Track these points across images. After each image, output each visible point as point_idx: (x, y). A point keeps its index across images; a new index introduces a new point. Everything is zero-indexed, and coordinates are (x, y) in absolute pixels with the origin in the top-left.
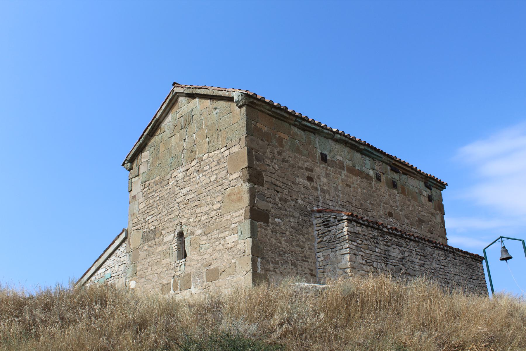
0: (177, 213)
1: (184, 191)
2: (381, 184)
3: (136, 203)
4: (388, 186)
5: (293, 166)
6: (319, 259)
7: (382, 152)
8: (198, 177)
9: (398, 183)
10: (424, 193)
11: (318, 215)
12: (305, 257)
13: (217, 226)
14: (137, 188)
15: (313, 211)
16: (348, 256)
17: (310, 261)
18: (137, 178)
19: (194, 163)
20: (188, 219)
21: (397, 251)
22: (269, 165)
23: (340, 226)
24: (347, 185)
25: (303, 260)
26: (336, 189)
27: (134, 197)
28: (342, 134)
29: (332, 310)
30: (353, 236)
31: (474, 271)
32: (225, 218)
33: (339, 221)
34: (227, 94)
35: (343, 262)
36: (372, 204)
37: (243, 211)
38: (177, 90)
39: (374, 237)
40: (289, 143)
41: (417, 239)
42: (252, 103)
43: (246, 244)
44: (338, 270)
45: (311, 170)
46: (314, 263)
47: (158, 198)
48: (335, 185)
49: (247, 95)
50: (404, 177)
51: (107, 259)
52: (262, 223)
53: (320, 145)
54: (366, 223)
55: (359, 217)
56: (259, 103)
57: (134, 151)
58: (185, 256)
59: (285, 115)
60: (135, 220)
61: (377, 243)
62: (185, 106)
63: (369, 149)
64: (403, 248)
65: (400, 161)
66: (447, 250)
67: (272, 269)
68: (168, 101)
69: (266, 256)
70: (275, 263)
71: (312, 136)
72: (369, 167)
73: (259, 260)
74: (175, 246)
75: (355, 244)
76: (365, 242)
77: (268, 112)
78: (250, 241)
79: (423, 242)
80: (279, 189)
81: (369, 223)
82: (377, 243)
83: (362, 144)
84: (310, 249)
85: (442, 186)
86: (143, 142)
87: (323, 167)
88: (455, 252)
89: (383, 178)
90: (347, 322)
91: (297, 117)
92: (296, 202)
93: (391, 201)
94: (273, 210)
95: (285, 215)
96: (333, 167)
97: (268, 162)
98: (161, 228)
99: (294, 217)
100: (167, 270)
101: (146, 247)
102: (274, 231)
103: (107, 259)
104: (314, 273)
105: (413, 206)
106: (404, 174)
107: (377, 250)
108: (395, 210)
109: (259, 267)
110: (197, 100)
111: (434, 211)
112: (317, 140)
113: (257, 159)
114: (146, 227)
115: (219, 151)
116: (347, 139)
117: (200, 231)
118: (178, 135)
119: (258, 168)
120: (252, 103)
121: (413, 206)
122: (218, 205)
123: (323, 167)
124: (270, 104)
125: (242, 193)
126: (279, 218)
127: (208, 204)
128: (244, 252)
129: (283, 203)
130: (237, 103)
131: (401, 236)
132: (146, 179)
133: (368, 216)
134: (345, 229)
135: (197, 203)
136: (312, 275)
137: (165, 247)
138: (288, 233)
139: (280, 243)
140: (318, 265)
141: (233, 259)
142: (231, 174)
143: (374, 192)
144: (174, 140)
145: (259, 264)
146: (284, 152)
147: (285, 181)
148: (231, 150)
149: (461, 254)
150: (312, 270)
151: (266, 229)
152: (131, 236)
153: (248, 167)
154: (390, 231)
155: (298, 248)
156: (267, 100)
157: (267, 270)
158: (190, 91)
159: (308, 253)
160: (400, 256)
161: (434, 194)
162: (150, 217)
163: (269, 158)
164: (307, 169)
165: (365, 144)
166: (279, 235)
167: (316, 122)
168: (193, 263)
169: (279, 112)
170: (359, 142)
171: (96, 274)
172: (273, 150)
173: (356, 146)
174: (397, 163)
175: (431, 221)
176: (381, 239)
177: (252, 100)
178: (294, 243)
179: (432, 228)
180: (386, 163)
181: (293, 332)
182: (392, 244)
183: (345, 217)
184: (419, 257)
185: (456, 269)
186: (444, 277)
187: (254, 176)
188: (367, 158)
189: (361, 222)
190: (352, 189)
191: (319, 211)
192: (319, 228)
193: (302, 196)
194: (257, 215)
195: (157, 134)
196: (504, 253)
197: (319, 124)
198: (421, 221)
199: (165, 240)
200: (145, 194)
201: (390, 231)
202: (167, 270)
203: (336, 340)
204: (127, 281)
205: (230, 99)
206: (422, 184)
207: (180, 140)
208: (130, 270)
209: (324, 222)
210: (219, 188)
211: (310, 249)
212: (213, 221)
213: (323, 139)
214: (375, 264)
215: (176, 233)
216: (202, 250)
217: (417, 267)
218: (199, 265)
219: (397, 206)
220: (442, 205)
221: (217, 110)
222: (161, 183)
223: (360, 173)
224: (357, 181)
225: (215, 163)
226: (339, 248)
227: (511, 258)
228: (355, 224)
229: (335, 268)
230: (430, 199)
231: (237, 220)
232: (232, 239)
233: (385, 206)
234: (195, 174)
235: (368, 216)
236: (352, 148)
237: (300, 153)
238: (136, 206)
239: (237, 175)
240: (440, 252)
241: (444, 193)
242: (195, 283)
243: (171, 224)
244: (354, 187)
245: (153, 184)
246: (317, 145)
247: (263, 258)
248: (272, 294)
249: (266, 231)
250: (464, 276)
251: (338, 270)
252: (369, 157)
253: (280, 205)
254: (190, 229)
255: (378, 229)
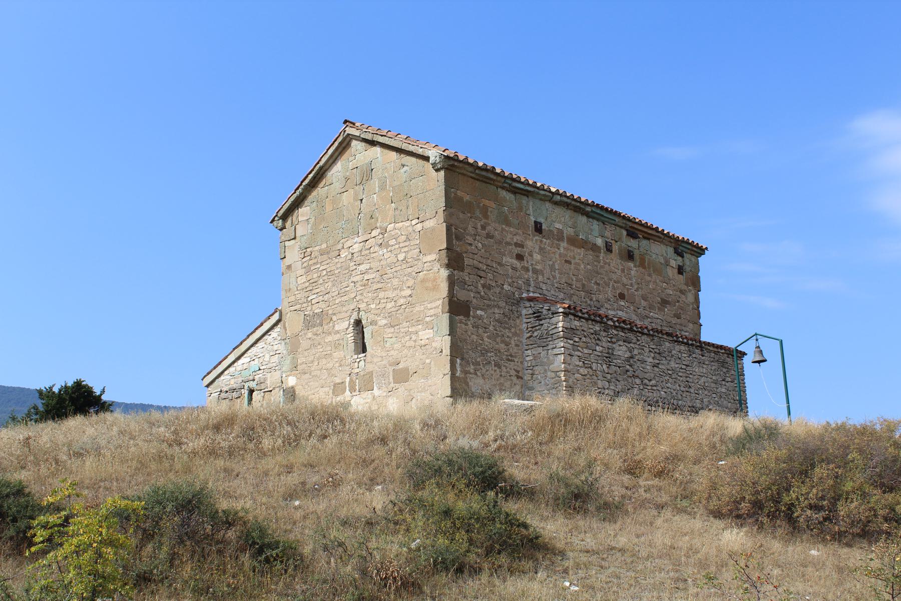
0: (353, 295)
1: (363, 268)
2: (612, 256)
3: (293, 275)
4: (621, 258)
5: (500, 242)
6: (528, 359)
7: (617, 214)
8: (381, 253)
9: (636, 253)
10: (673, 263)
11: (528, 304)
12: (511, 355)
13: (407, 317)
14: (293, 255)
15: (522, 299)
16: (562, 357)
17: (516, 360)
18: (293, 241)
19: (374, 233)
20: (368, 305)
21: (624, 348)
22: (471, 245)
23: (554, 320)
24: (566, 261)
25: (508, 360)
26: (552, 268)
27: (289, 267)
28: (564, 195)
29: (538, 429)
30: (570, 332)
31: (729, 370)
32: (417, 309)
33: (553, 314)
34: (420, 151)
35: (556, 364)
36: (598, 284)
37: (440, 302)
38: (349, 130)
39: (595, 333)
40: (496, 211)
41: (651, 332)
42: (453, 166)
43: (444, 343)
44: (549, 373)
45: (522, 246)
46: (522, 363)
47: (325, 272)
48: (551, 263)
49: (447, 157)
50: (645, 243)
51: (252, 346)
52: (462, 317)
53: (534, 211)
54: (586, 316)
55: (578, 309)
56: (461, 165)
57: (287, 205)
58: (364, 350)
59: (492, 176)
60: (292, 298)
61: (599, 339)
62: (359, 154)
63: (598, 211)
64: (632, 345)
65: (640, 223)
66: (692, 345)
67: (472, 371)
68: (336, 144)
69: (466, 356)
70: (478, 364)
71: (524, 200)
72: (596, 233)
73: (458, 361)
74: (350, 336)
75: (571, 342)
76: (584, 339)
77: (473, 175)
78: (448, 338)
79: (660, 335)
80: (482, 274)
81: (589, 315)
82: (599, 339)
83: (589, 205)
84: (517, 345)
85: (699, 251)
86: (301, 194)
87: (536, 240)
88: (704, 347)
89: (615, 248)
90: (551, 439)
91: (506, 177)
92: (502, 289)
93: (624, 278)
94: (474, 301)
95: (488, 306)
96: (548, 238)
97: (470, 239)
98: (330, 312)
99: (499, 307)
100: (341, 366)
101: (310, 335)
102: (476, 326)
103: (252, 346)
104: (520, 375)
105: (655, 282)
106: (645, 238)
107: (598, 348)
108: (628, 289)
109: (459, 369)
110: (378, 149)
111: (684, 287)
112: (531, 203)
113: (458, 238)
114: (309, 308)
115: (408, 224)
116: (569, 201)
117: (384, 322)
118: (351, 191)
119: (458, 249)
120: (453, 166)
121: (655, 282)
122: (409, 292)
123: (536, 240)
124: (474, 166)
125: (439, 281)
126: (481, 310)
127: (395, 289)
128: (441, 352)
129: (486, 291)
130: (434, 165)
131: (631, 330)
132: (306, 246)
133: (591, 300)
134: (561, 324)
135: (379, 286)
136: (518, 377)
137: (337, 336)
138: (491, 328)
139: (482, 340)
140: (526, 365)
141: (427, 358)
142: (425, 255)
143: (602, 267)
144: (346, 198)
145: (458, 366)
146: (489, 224)
147: (489, 262)
148: (424, 223)
149: (711, 348)
150: (518, 372)
151: (466, 325)
152: (287, 318)
153: (447, 249)
154: (617, 324)
155: (503, 345)
156: (471, 161)
157: (466, 372)
158: (369, 137)
159: (514, 350)
160: (628, 355)
161: (687, 262)
162: (314, 296)
163: (471, 235)
164: (517, 245)
165: (593, 205)
166: (481, 331)
167: (531, 182)
168: (375, 360)
169: (484, 173)
170: (586, 203)
171: (236, 364)
172: (476, 224)
173: (580, 208)
174: (635, 226)
175: (678, 301)
176: (604, 334)
177: (451, 162)
178: (498, 339)
179: (680, 311)
180: (621, 227)
181: (506, 448)
182: (618, 340)
183: (561, 310)
184: (652, 355)
185: (703, 371)
186: (684, 379)
187: (454, 260)
188: (595, 222)
189: (580, 315)
190: (572, 266)
191: (530, 299)
192: (529, 320)
193: (510, 280)
194: (457, 308)
195: (321, 185)
196: (757, 355)
197: (534, 185)
198: (664, 302)
199: (337, 328)
200: (305, 264)
201: (617, 324)
202: (341, 366)
203: (541, 454)
204: (284, 376)
205: (426, 159)
206: (671, 250)
207: (355, 200)
208: (288, 362)
209: (534, 313)
210: (410, 270)
211: (517, 345)
212: (401, 311)
213: (538, 202)
214: (594, 366)
215: (352, 321)
216: (388, 345)
217: (648, 367)
218: (383, 363)
219: (631, 285)
220: (699, 277)
221: (406, 168)
222: (328, 253)
223: (583, 244)
224: (580, 254)
225: (404, 238)
226: (552, 346)
227: (765, 361)
228: (572, 317)
229: (545, 370)
230: (680, 270)
231: (432, 312)
232: (425, 334)
233: (616, 285)
234: (377, 248)
235: (591, 300)
236: (575, 211)
237: (509, 224)
238: (293, 280)
239: (433, 257)
240: (683, 348)
241: (701, 260)
242: (378, 383)
243: (344, 309)
244: (576, 264)
245: (317, 254)
246: (531, 211)
247: (462, 359)
248: (487, 412)
249: (466, 327)
250: (714, 378)
251: (549, 373)
252: (598, 220)
253: (482, 294)
254: (371, 317)
255: (601, 323)
